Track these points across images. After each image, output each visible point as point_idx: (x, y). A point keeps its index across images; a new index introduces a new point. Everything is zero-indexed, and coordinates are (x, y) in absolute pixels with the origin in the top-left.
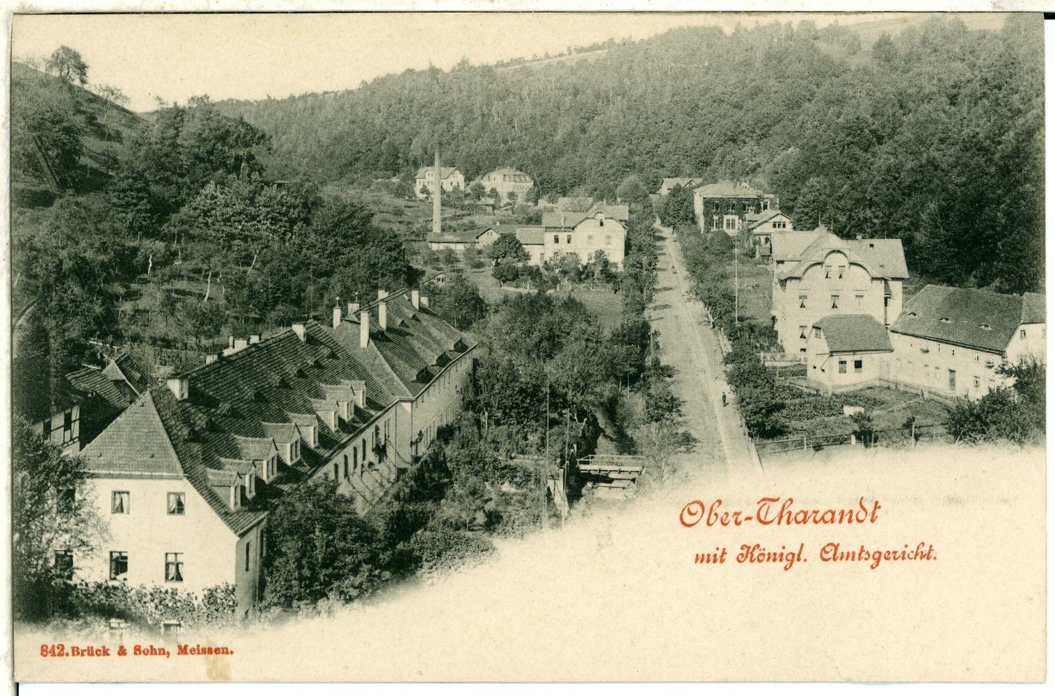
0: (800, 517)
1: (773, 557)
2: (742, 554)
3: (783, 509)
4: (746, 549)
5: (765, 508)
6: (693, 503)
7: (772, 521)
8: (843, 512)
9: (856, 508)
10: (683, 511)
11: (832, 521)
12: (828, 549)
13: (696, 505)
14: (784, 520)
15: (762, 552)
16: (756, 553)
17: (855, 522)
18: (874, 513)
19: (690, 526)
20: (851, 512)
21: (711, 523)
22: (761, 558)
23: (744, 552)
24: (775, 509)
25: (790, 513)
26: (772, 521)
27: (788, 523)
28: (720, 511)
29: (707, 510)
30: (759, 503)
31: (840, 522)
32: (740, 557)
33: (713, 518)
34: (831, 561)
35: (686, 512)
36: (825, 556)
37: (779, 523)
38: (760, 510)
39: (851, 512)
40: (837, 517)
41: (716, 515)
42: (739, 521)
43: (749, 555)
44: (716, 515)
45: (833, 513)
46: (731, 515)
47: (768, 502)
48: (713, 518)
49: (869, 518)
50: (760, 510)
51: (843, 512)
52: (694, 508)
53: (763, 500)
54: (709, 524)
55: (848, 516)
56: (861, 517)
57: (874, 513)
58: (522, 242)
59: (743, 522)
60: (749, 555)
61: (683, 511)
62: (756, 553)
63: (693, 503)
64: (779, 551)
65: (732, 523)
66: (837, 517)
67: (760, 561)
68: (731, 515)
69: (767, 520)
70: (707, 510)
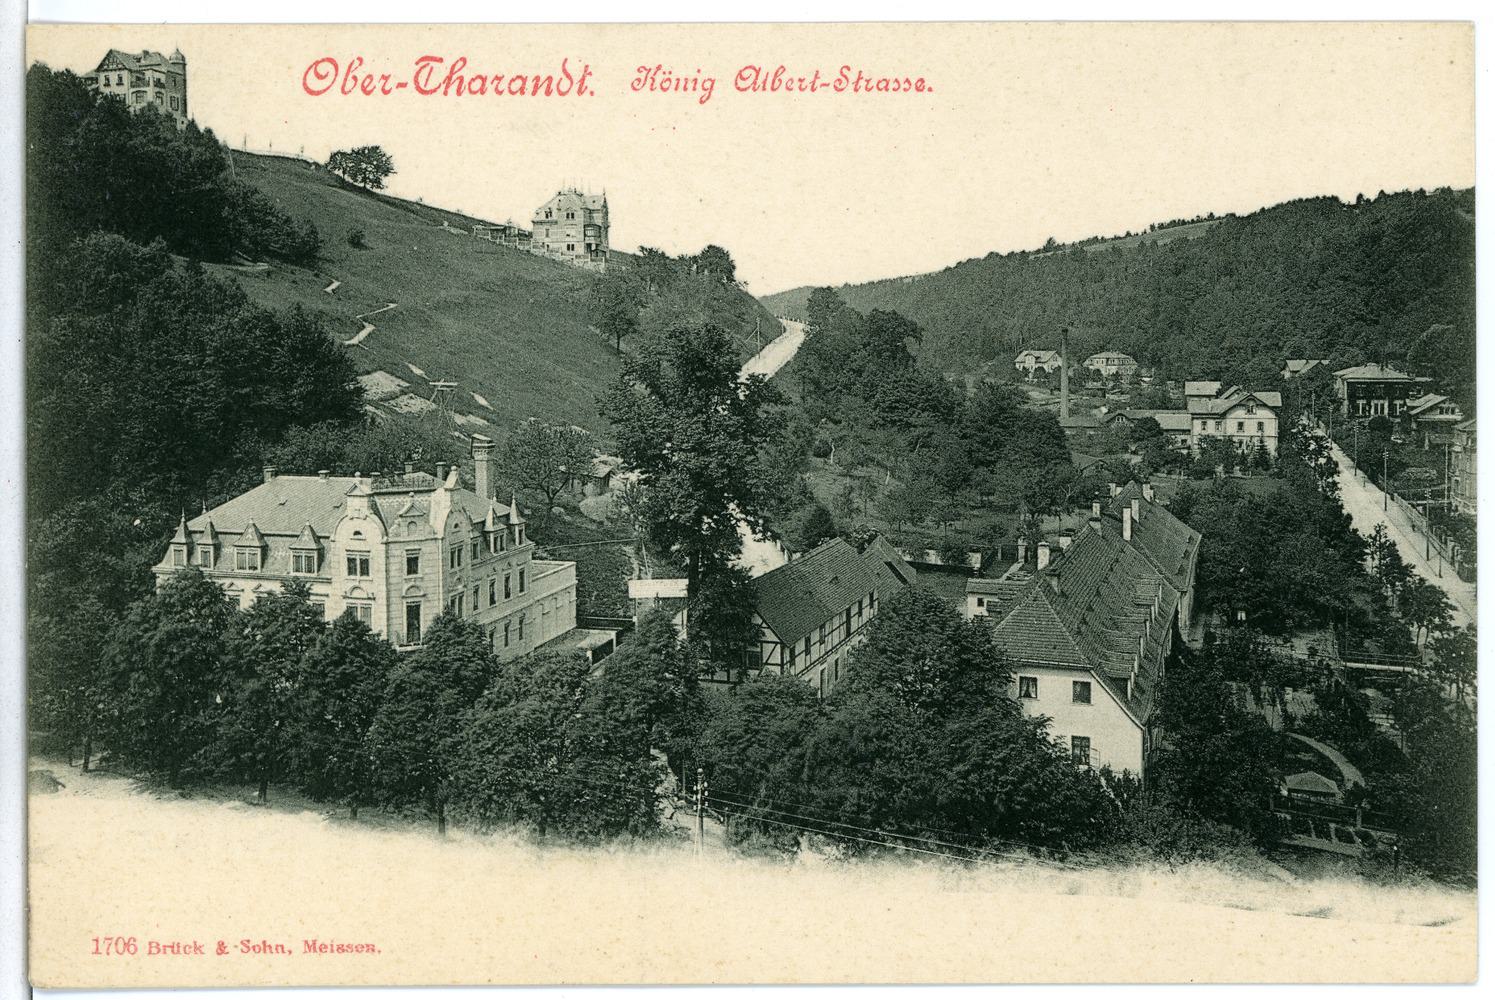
0: (476, 85)
1: (682, 85)
2: (639, 80)
3: (452, 72)
4: (645, 73)
5: (425, 72)
6: (323, 60)
7: (435, 91)
8: (537, 78)
9: (557, 75)
10: (307, 73)
11: (522, 91)
12: (746, 74)
13: (326, 64)
14: (453, 89)
15: (667, 76)
16: (659, 77)
17: (555, 93)
18: (583, 80)
19: (318, 93)
20: (550, 79)
21: (346, 89)
22: (665, 85)
23: (642, 76)
24: (440, 72)
25: (461, 79)
26: (435, 91)
27: (459, 93)
28: (361, 74)
29: (343, 70)
30: (417, 63)
31: (534, 93)
32: (636, 83)
33: (350, 84)
34: (750, 90)
35: (311, 73)
36: (742, 84)
37: (445, 93)
38: (418, 73)
39: (550, 79)
40: (530, 86)
41: (355, 78)
42: (387, 88)
43: (649, 81)
44: (355, 78)
45: (524, 80)
46: (377, 77)
47: (432, 64)
48: (350, 84)
49: (576, 87)
50: (418, 73)
51: (537, 78)
52: (323, 68)
53: (422, 59)
54: (344, 92)
55: (545, 85)
56: (563, 88)
57: (583, 80)
58: (759, 608)
59: (394, 90)
60: (649, 81)
61: (307, 73)
62: (659, 77)
63: (323, 60)
64: (693, 74)
65: (378, 92)
66: (530, 86)
67: (664, 90)
68: (377, 77)
69: (428, 88)
70: (343, 70)
